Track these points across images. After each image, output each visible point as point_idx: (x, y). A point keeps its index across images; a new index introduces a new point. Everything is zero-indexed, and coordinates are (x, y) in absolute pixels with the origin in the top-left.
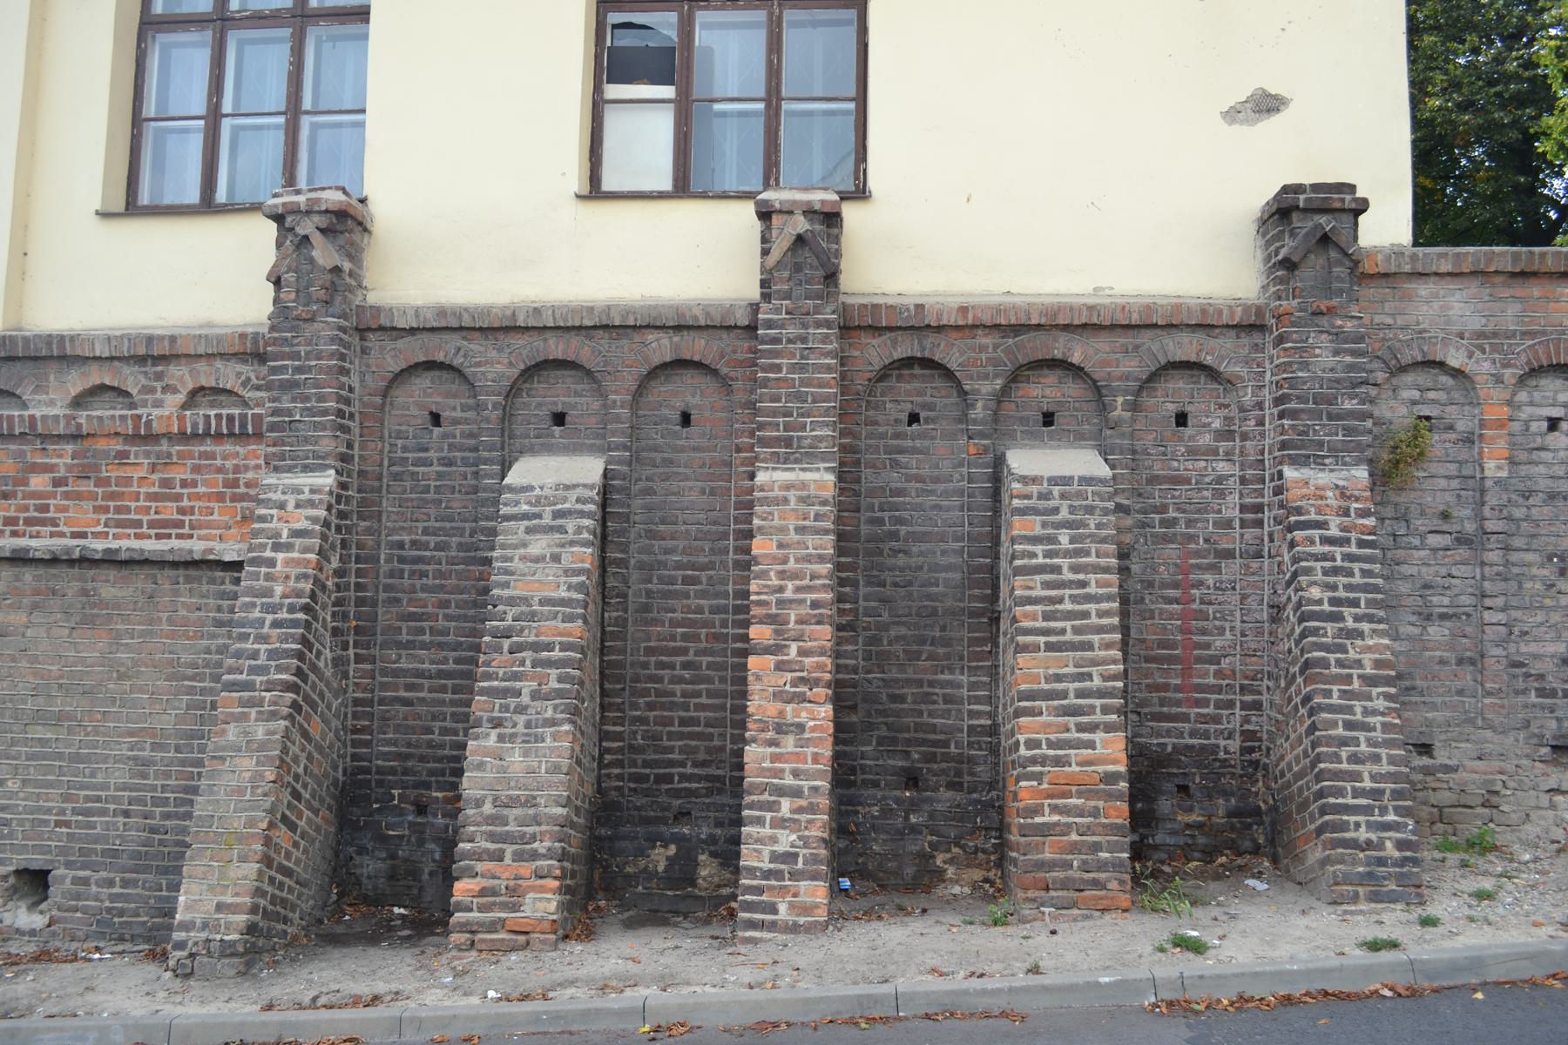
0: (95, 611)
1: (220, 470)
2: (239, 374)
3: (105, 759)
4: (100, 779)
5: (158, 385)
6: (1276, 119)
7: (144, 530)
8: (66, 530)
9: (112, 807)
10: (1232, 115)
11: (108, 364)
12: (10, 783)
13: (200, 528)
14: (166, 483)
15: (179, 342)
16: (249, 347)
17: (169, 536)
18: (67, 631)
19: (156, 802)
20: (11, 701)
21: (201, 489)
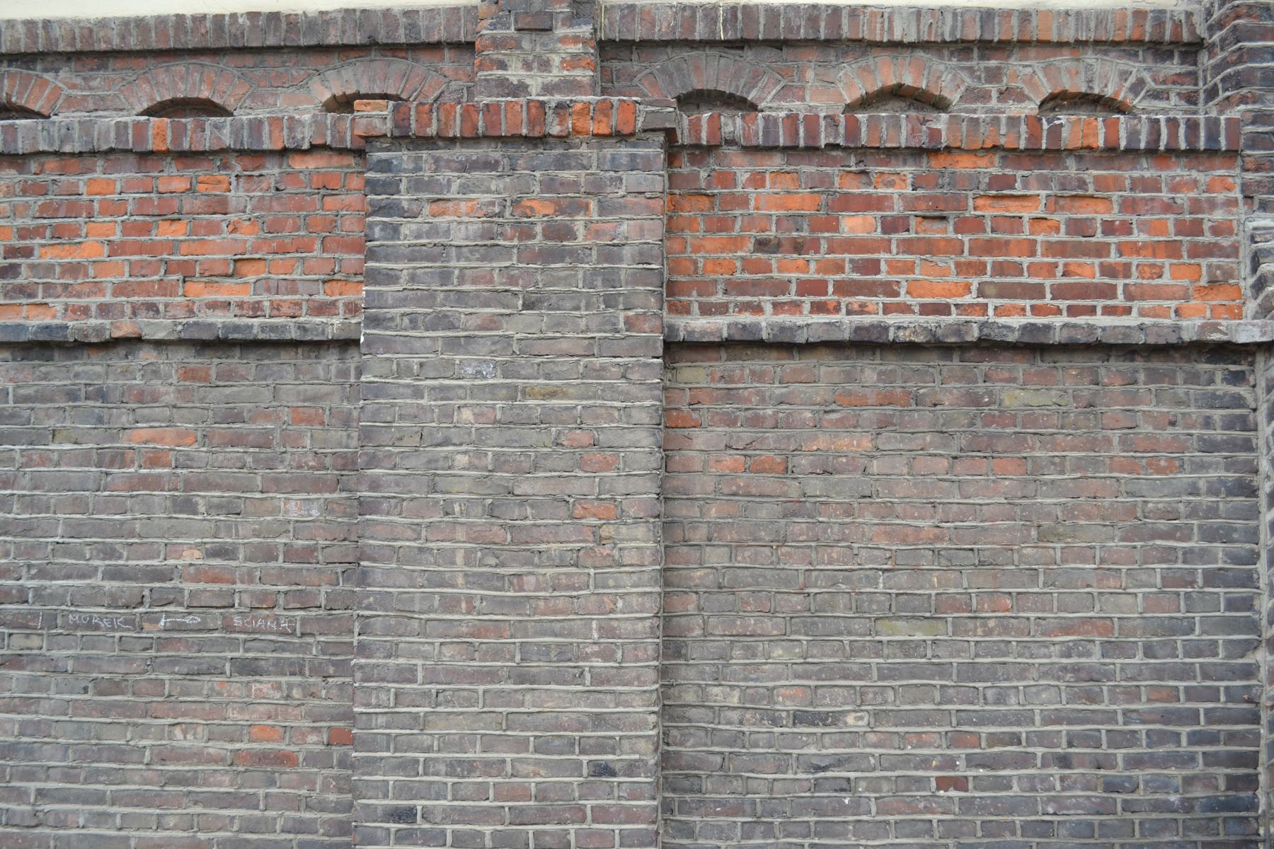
0: (993, 429)
1: (1169, 207)
2: (1124, 75)
3: (1022, 672)
4: (1013, 705)
5: (993, 89)
7: (1048, 300)
8: (913, 301)
9: (1040, 751)
11: (907, 53)
12: (850, 719)
13: (1142, 297)
14: (1078, 227)
15: (1035, 21)
16: (1148, 34)
17: (1092, 311)
18: (945, 463)
19: (1117, 739)
20: (847, 581)
21: (1139, 237)
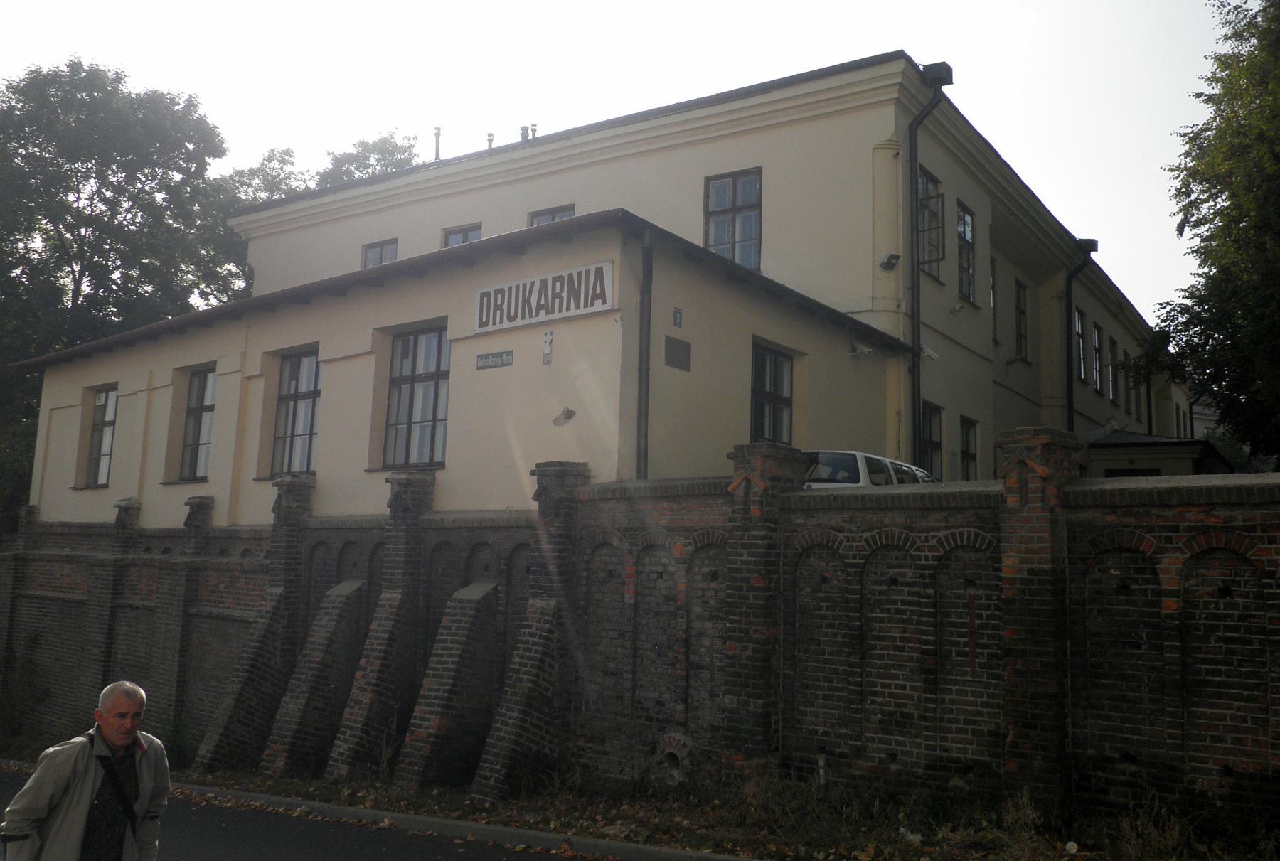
6: (571, 421)
10: (556, 422)
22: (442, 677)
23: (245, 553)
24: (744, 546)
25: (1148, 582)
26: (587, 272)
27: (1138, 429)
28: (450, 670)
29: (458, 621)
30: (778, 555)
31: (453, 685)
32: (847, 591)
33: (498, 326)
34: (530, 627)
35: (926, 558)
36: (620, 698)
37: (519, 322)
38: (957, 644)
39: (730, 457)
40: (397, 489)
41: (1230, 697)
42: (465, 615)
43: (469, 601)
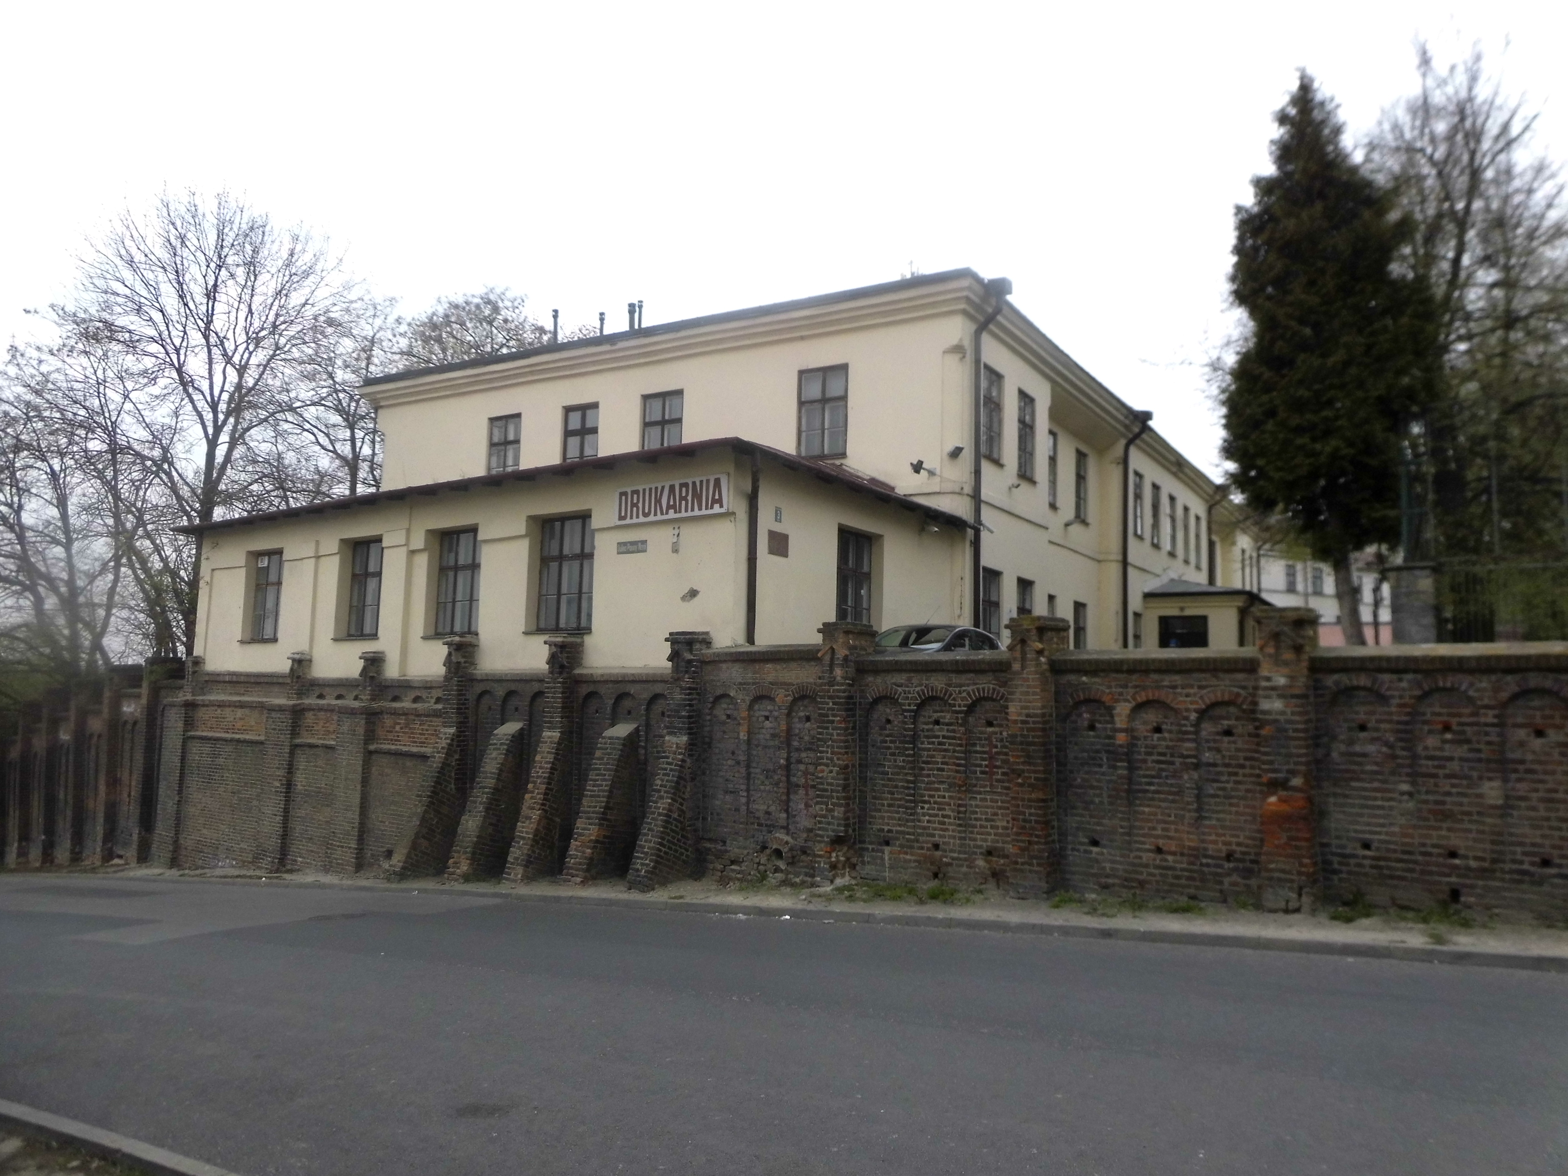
6: (696, 599)
10: (683, 598)
22: (599, 796)
23: (416, 700)
24: (830, 697)
25: (1108, 722)
26: (708, 481)
27: (1200, 579)
28: (604, 791)
29: (609, 754)
30: (855, 704)
31: (607, 802)
32: (905, 730)
33: (635, 520)
34: (667, 757)
35: (960, 706)
36: (737, 810)
37: (652, 518)
38: (981, 766)
39: (819, 631)
40: (554, 649)
41: (1160, 800)
42: (614, 749)
43: (618, 738)
